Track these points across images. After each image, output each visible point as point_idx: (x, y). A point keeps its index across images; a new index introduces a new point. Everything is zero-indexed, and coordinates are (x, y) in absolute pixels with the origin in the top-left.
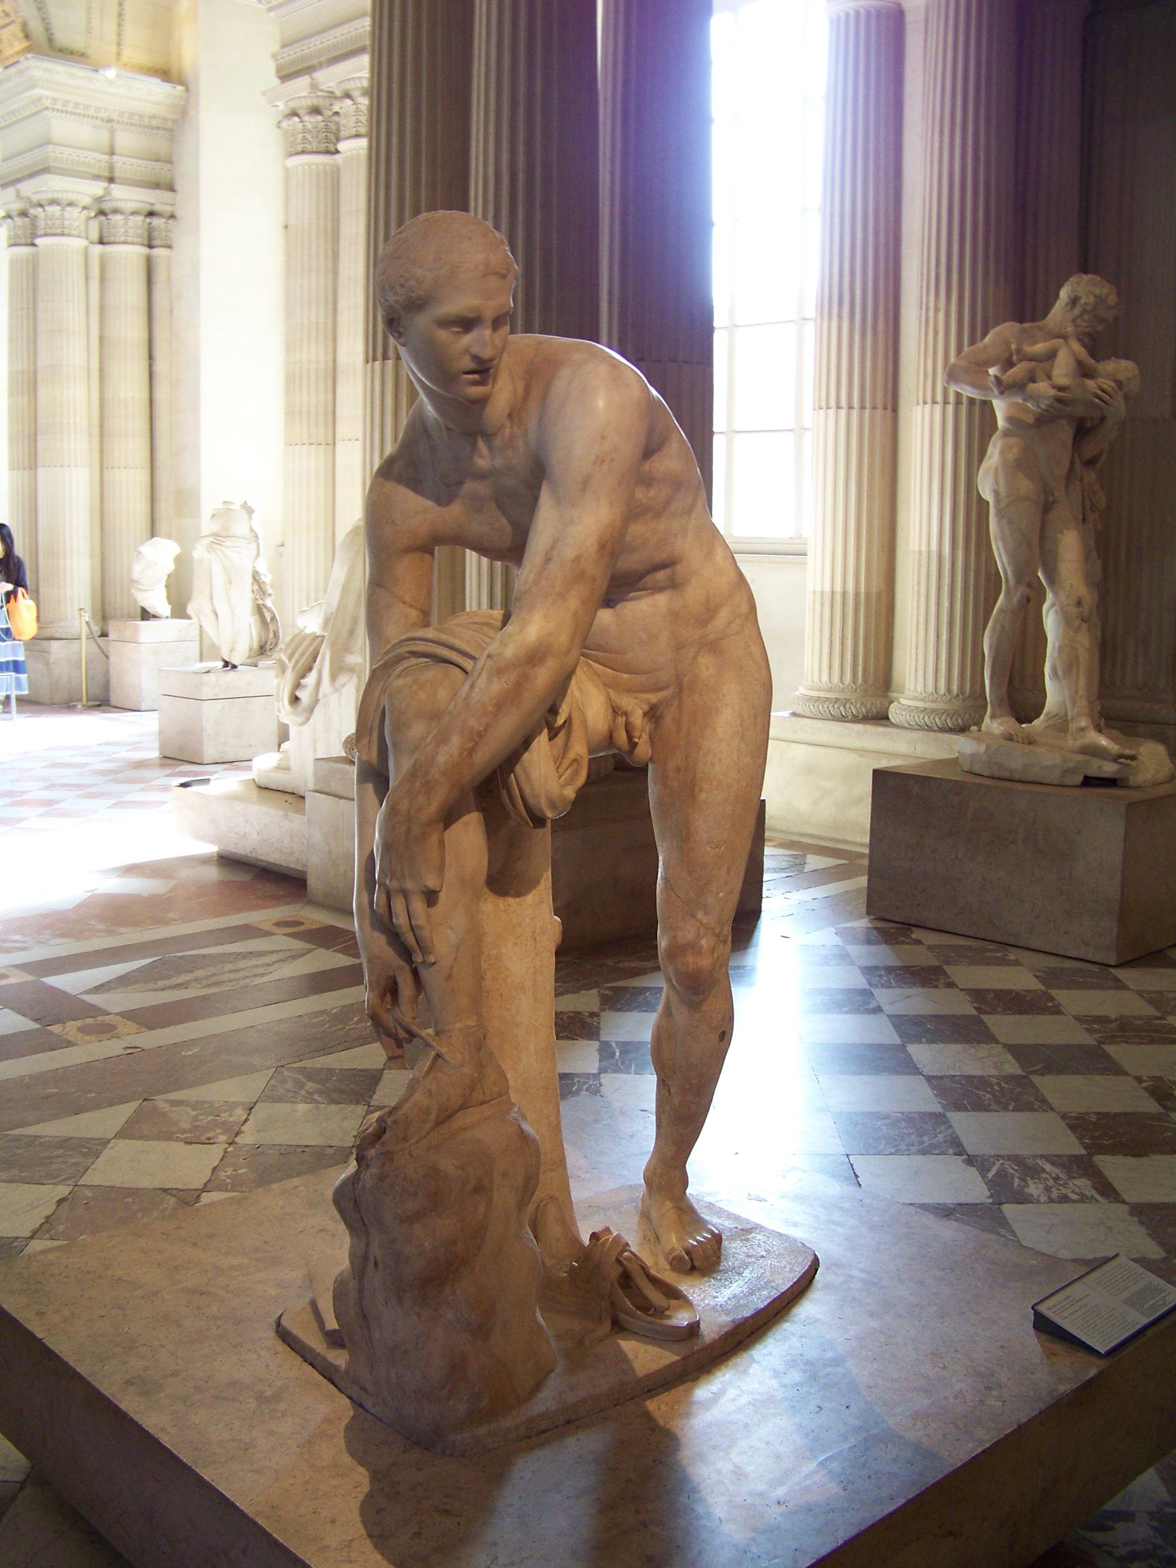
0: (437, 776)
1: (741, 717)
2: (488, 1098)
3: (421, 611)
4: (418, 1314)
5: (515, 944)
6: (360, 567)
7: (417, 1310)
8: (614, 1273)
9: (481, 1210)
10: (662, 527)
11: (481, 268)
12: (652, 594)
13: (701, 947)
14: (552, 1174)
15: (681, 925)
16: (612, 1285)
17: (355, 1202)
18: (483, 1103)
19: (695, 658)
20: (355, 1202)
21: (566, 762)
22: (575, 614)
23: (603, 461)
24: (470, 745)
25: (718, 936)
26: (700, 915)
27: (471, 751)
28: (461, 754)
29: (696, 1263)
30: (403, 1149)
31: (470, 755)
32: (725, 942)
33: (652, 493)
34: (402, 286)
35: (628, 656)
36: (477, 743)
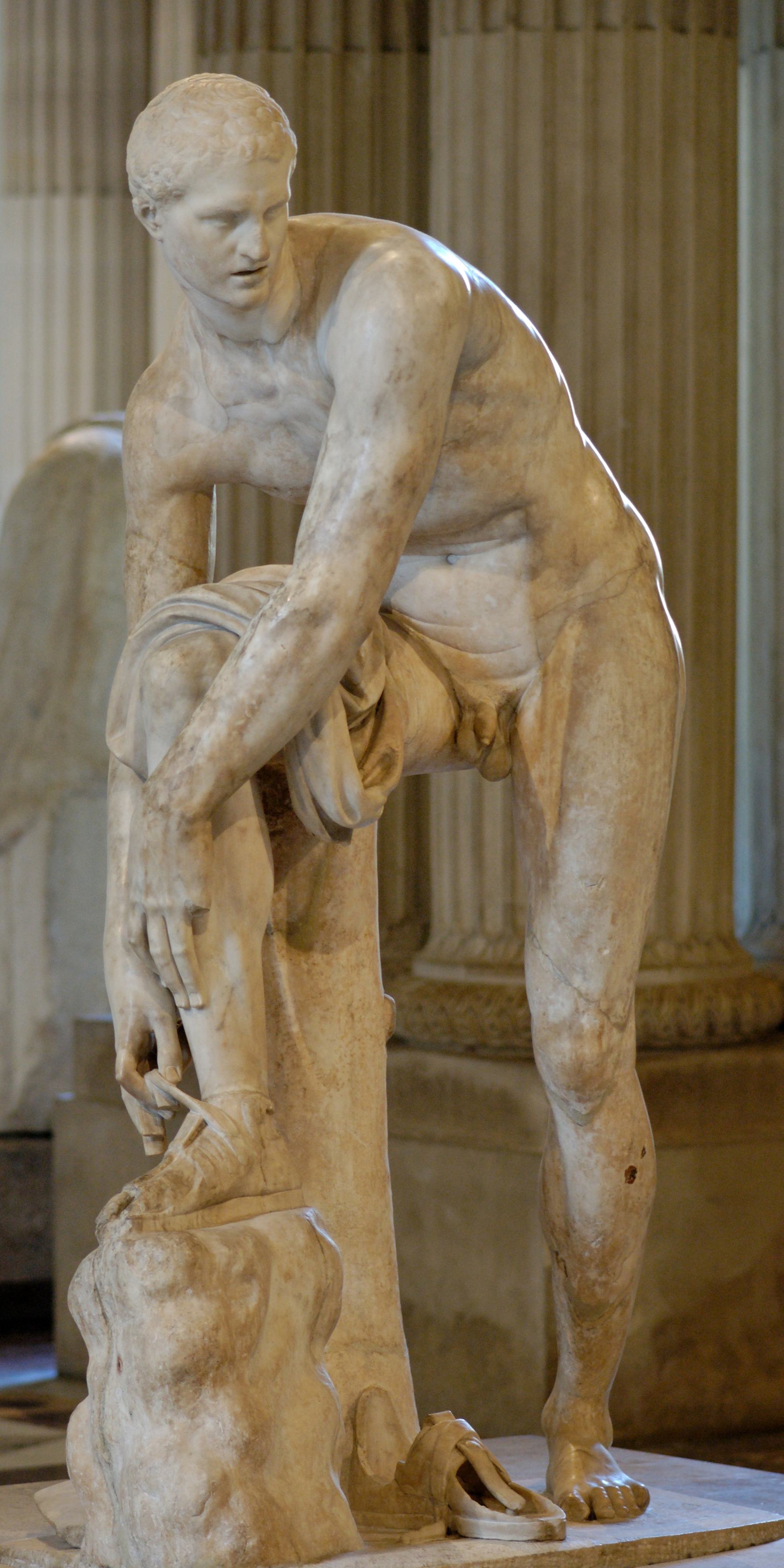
0: (201, 761)
1: (623, 707)
2: (270, 1187)
3: (195, 569)
4: (171, 1423)
5: (323, 1018)
6: (452, 706)
7: (169, 1417)
8: (453, 1462)
9: (253, 1302)
10: (504, 457)
11: (249, 153)
12: (502, 544)
13: (581, 1027)
14: (381, 1358)
15: (552, 997)
16: (449, 1479)
17: (96, 1289)
18: (263, 1193)
19: (561, 629)
20: (96, 1289)
21: (374, 758)
22: (367, 564)
23: (399, 378)
24: (241, 722)
25: (607, 1013)
26: (577, 981)
27: (241, 730)
28: (230, 734)
29: (597, 1511)
30: (155, 1218)
31: (241, 734)
32: (622, 1027)
33: (486, 411)
34: (157, 173)
35: (474, 629)
36: (248, 720)
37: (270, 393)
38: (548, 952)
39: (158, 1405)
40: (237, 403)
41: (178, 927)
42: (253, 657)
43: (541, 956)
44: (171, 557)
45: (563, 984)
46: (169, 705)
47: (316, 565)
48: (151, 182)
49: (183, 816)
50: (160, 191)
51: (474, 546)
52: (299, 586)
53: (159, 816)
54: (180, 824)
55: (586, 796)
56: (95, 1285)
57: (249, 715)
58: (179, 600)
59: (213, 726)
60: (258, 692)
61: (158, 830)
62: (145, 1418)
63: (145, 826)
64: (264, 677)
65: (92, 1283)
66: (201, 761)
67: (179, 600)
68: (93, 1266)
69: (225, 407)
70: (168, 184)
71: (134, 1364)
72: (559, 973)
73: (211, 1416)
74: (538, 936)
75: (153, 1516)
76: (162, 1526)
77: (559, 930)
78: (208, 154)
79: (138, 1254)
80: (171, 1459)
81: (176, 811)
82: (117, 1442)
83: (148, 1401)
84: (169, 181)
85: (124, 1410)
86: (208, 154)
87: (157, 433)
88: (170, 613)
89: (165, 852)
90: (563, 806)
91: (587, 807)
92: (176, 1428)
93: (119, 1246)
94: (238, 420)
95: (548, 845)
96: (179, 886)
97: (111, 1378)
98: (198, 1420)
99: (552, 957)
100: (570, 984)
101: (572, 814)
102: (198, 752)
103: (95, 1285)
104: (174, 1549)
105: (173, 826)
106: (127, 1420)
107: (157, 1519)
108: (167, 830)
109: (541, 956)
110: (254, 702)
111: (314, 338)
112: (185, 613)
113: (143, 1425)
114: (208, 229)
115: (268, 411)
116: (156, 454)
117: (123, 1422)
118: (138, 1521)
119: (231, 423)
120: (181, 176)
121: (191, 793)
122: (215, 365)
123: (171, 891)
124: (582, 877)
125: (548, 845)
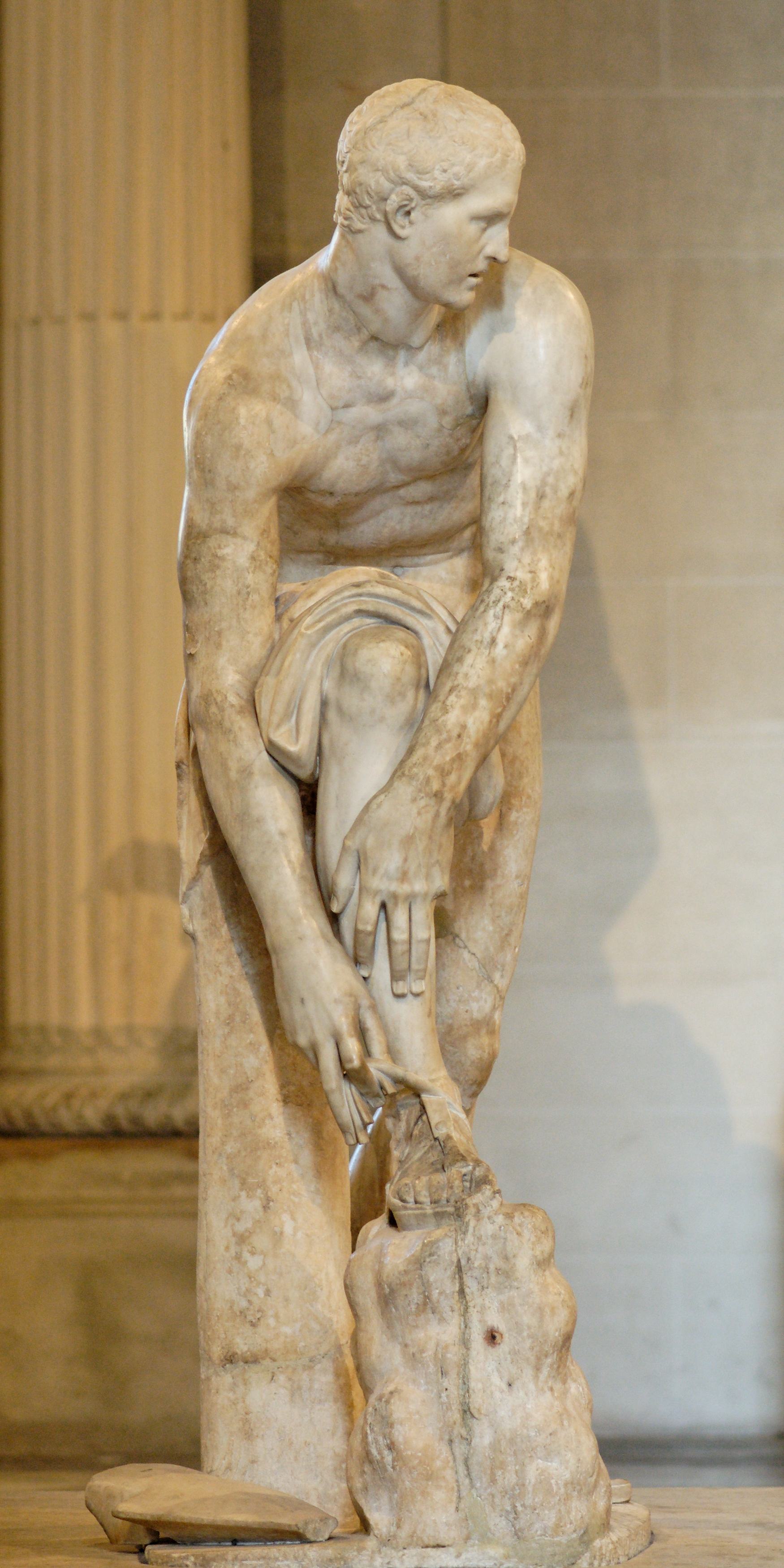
4: (551, 1389)
17: (459, 1268)
20: (459, 1268)
28: (491, 722)
37: (383, 398)
38: (474, 950)
39: (545, 1371)
40: (347, 406)
41: (423, 915)
42: (506, 646)
43: (466, 955)
44: (271, 557)
45: (486, 981)
46: (402, 695)
47: (539, 560)
48: (435, 179)
49: (453, 802)
50: (443, 188)
51: (429, 558)
52: (533, 580)
53: (432, 802)
54: (450, 809)
55: (524, 799)
56: (459, 1261)
57: (505, 703)
58: (360, 595)
59: (477, 714)
60: (513, 680)
61: (429, 816)
62: (531, 1386)
63: (415, 811)
64: (517, 666)
65: (455, 1260)
66: (469, 747)
67: (360, 595)
68: (456, 1243)
69: (333, 409)
70: (456, 182)
71: (525, 1334)
72: (483, 970)
73: (575, 1381)
74: (463, 935)
75: (553, 1481)
76: (562, 1490)
77: (491, 928)
78: (499, 155)
79: (520, 1225)
80: (566, 1423)
81: (448, 796)
82: (486, 1415)
83: (538, 1369)
84: (458, 180)
85: (498, 1382)
86: (499, 155)
87: (273, 432)
88: (355, 607)
89: (430, 838)
90: (504, 810)
91: (525, 810)
92: (556, 1395)
93: (500, 1219)
94: (339, 423)
95: (485, 847)
96: (436, 872)
97: (473, 1353)
98: (567, 1386)
99: (479, 955)
100: (492, 982)
101: (513, 816)
102: (466, 739)
103: (459, 1261)
104: (569, 1512)
105: (443, 812)
106: (502, 1392)
107: (557, 1484)
108: (437, 815)
109: (466, 955)
110: (510, 690)
111: (462, 345)
112: (370, 607)
113: (526, 1394)
114: (473, 228)
115: (373, 414)
116: (272, 454)
117: (497, 1395)
118: (530, 1488)
119: (334, 424)
120: (471, 175)
121: (460, 778)
122: (329, 367)
123: (428, 877)
124: (517, 877)
125: (485, 847)
